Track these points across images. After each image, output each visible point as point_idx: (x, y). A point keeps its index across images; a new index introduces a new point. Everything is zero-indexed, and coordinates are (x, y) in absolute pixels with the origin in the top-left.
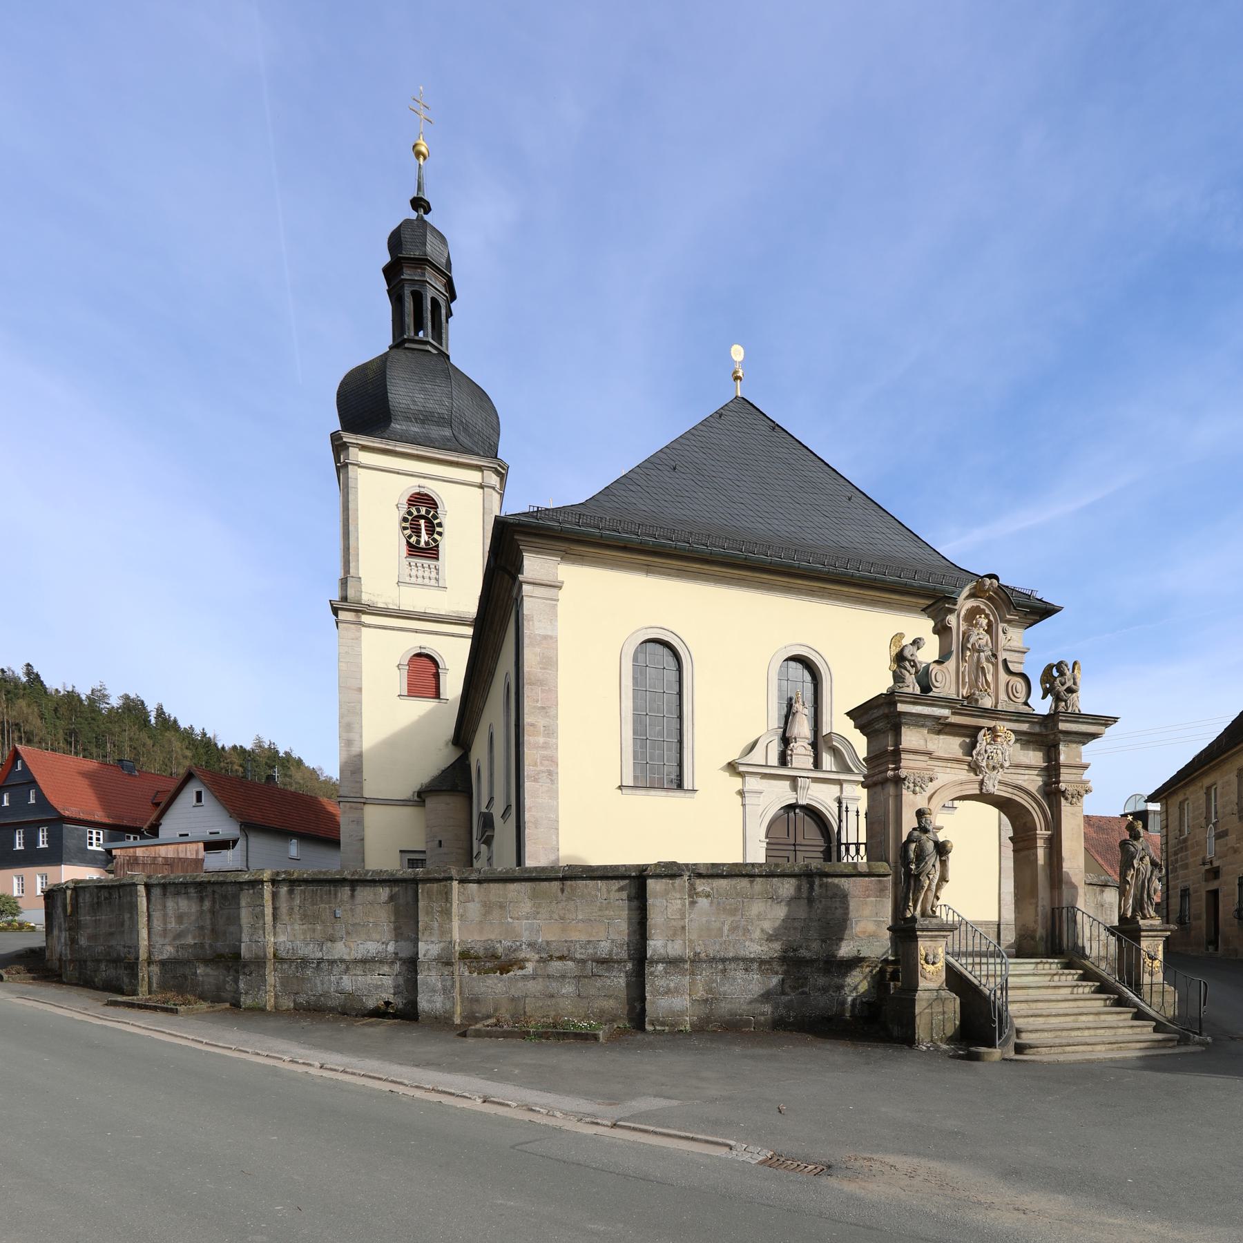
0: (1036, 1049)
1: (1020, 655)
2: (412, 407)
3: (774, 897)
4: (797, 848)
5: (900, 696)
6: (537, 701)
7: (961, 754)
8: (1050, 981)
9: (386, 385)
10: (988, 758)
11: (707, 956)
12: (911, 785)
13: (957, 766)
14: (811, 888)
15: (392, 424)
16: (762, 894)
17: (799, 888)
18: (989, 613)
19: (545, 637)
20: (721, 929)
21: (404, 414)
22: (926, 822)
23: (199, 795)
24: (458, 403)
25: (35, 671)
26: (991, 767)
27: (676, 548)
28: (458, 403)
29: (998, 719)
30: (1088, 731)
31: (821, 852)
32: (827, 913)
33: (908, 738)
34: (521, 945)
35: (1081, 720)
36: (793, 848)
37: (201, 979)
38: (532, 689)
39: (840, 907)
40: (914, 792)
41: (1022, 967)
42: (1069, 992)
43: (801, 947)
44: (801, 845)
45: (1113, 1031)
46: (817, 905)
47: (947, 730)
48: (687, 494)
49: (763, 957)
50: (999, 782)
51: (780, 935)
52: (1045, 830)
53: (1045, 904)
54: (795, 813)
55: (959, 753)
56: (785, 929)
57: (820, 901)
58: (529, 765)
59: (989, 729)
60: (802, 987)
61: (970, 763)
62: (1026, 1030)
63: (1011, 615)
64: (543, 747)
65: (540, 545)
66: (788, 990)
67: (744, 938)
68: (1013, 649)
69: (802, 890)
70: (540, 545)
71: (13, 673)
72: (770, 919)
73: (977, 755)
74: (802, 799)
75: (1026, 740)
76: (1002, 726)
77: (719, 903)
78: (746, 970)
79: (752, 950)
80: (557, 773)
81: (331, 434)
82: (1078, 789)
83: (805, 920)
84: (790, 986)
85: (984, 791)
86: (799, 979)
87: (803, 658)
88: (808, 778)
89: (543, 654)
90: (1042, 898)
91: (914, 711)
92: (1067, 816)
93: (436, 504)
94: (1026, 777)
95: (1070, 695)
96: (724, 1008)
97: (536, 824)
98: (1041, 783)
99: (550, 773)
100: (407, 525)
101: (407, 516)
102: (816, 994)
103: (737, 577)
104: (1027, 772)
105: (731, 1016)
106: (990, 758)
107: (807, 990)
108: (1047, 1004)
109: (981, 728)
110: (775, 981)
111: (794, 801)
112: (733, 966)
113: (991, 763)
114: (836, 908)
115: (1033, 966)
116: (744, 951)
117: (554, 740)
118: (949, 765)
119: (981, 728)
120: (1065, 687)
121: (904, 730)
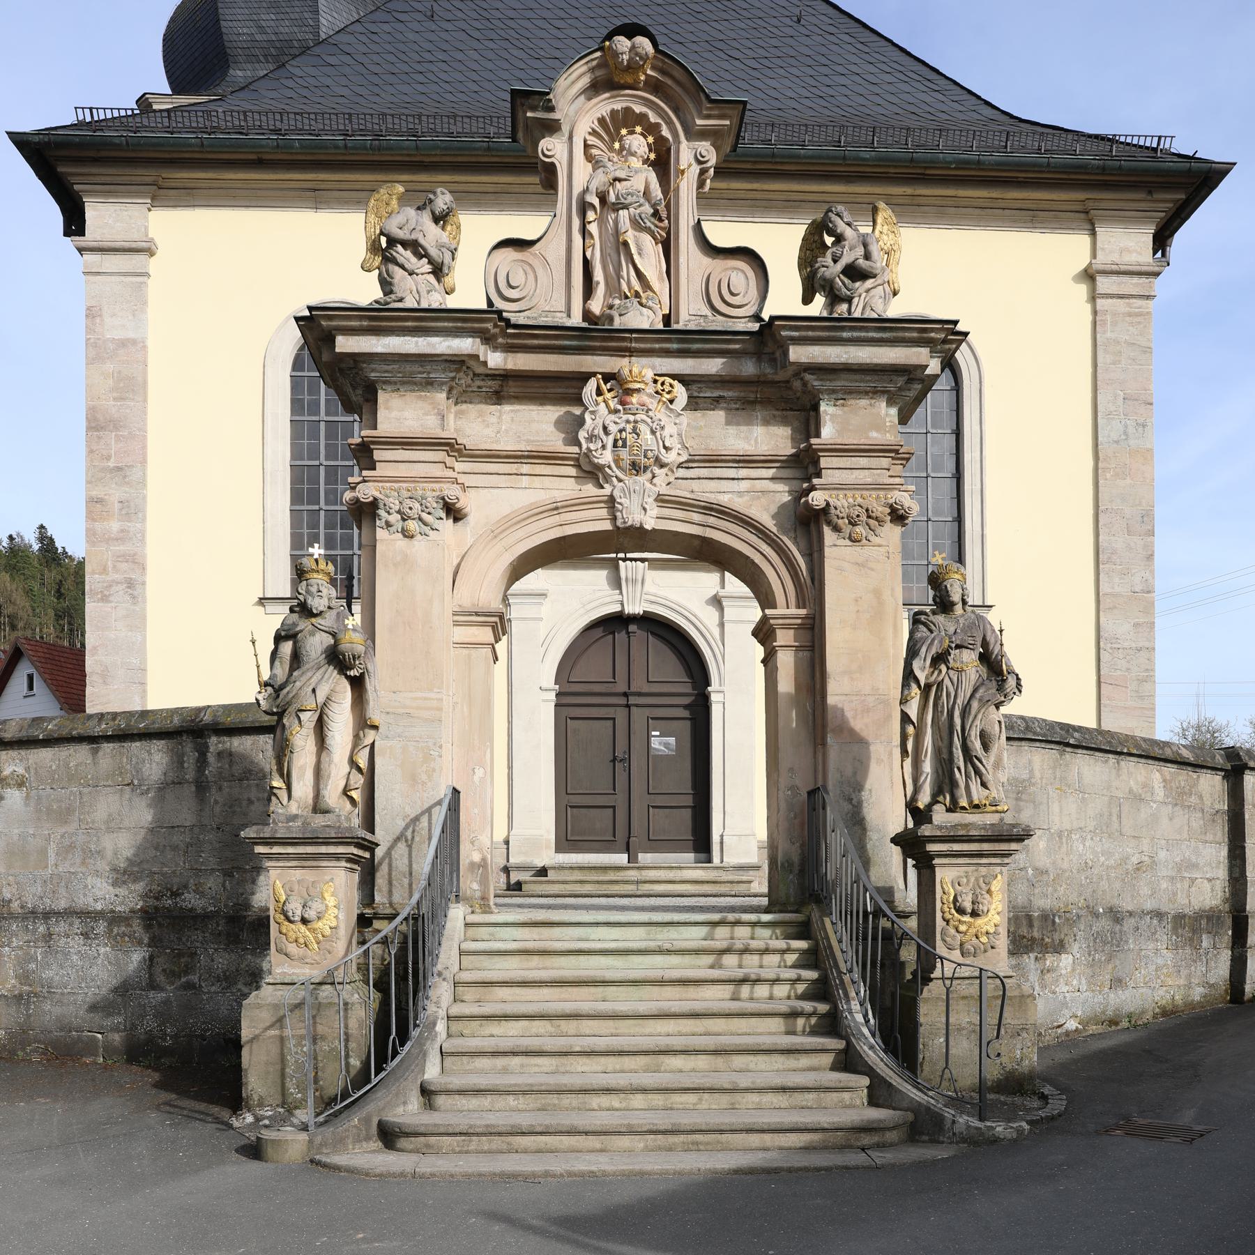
0: (422, 1139)
1: (1143, 280)
2: (258, 37)
3: (136, 782)
4: (632, 700)
5: (330, 318)
6: (108, 458)
7: (560, 443)
8: (712, 967)
9: (217, 9)
10: (615, 446)
11: (22, 907)
12: (394, 518)
14: (202, 761)
15: (231, 71)
16: (114, 775)
17: (178, 761)
18: (660, 121)
19: (123, 343)
20: (43, 852)
21: (247, 52)
22: (308, 592)
23: (30, 678)
24: (330, 19)
25: (49, 534)
26: (626, 463)
27: (346, 147)
28: (330, 19)
29: (631, 352)
30: (876, 361)
31: (686, 707)
33: (394, 414)
35: (845, 335)
36: (623, 701)
38: (99, 438)
39: (258, 800)
40: (407, 535)
41: (673, 933)
42: (728, 996)
43: (186, 887)
44: (640, 694)
45: (724, 1100)
46: (214, 795)
47: (512, 388)
48: (441, 56)
49: (118, 909)
50: (656, 500)
51: (148, 861)
52: (798, 607)
53: (798, 782)
54: (628, 633)
55: (555, 442)
56: (156, 849)
57: (220, 789)
58: (93, 573)
59: (607, 377)
60: (186, 973)
61: (577, 460)
62: (443, 1088)
63: (708, 117)
64: (117, 539)
65: (108, 179)
66: (160, 978)
67: (84, 870)
68: (1123, 268)
69: (186, 765)
70: (108, 179)
71: (22, 540)
72: (128, 829)
73: (591, 438)
74: (634, 603)
75: (738, 399)
76: (642, 369)
77: (39, 798)
78: (85, 935)
79: (99, 894)
80: (144, 583)
81: (137, 102)
82: (865, 504)
84: (164, 970)
85: (619, 523)
86: (180, 955)
88: (643, 560)
89: (120, 372)
90: (791, 770)
91: (379, 349)
92: (840, 569)
94: (744, 485)
95: (858, 284)
96: (49, 1012)
97: (105, 677)
98: (786, 498)
99: (130, 584)
102: (213, 989)
103: (490, 188)
104: (743, 473)
105: (61, 1030)
106: (620, 443)
107: (196, 980)
108: (610, 1023)
109: (585, 377)
110: (137, 957)
111: (617, 608)
112: (62, 927)
113: (624, 454)
114: (250, 802)
115: (703, 931)
116: (85, 895)
117: (138, 525)
118: (525, 469)
119: (585, 377)
120: (840, 266)
121: (381, 396)
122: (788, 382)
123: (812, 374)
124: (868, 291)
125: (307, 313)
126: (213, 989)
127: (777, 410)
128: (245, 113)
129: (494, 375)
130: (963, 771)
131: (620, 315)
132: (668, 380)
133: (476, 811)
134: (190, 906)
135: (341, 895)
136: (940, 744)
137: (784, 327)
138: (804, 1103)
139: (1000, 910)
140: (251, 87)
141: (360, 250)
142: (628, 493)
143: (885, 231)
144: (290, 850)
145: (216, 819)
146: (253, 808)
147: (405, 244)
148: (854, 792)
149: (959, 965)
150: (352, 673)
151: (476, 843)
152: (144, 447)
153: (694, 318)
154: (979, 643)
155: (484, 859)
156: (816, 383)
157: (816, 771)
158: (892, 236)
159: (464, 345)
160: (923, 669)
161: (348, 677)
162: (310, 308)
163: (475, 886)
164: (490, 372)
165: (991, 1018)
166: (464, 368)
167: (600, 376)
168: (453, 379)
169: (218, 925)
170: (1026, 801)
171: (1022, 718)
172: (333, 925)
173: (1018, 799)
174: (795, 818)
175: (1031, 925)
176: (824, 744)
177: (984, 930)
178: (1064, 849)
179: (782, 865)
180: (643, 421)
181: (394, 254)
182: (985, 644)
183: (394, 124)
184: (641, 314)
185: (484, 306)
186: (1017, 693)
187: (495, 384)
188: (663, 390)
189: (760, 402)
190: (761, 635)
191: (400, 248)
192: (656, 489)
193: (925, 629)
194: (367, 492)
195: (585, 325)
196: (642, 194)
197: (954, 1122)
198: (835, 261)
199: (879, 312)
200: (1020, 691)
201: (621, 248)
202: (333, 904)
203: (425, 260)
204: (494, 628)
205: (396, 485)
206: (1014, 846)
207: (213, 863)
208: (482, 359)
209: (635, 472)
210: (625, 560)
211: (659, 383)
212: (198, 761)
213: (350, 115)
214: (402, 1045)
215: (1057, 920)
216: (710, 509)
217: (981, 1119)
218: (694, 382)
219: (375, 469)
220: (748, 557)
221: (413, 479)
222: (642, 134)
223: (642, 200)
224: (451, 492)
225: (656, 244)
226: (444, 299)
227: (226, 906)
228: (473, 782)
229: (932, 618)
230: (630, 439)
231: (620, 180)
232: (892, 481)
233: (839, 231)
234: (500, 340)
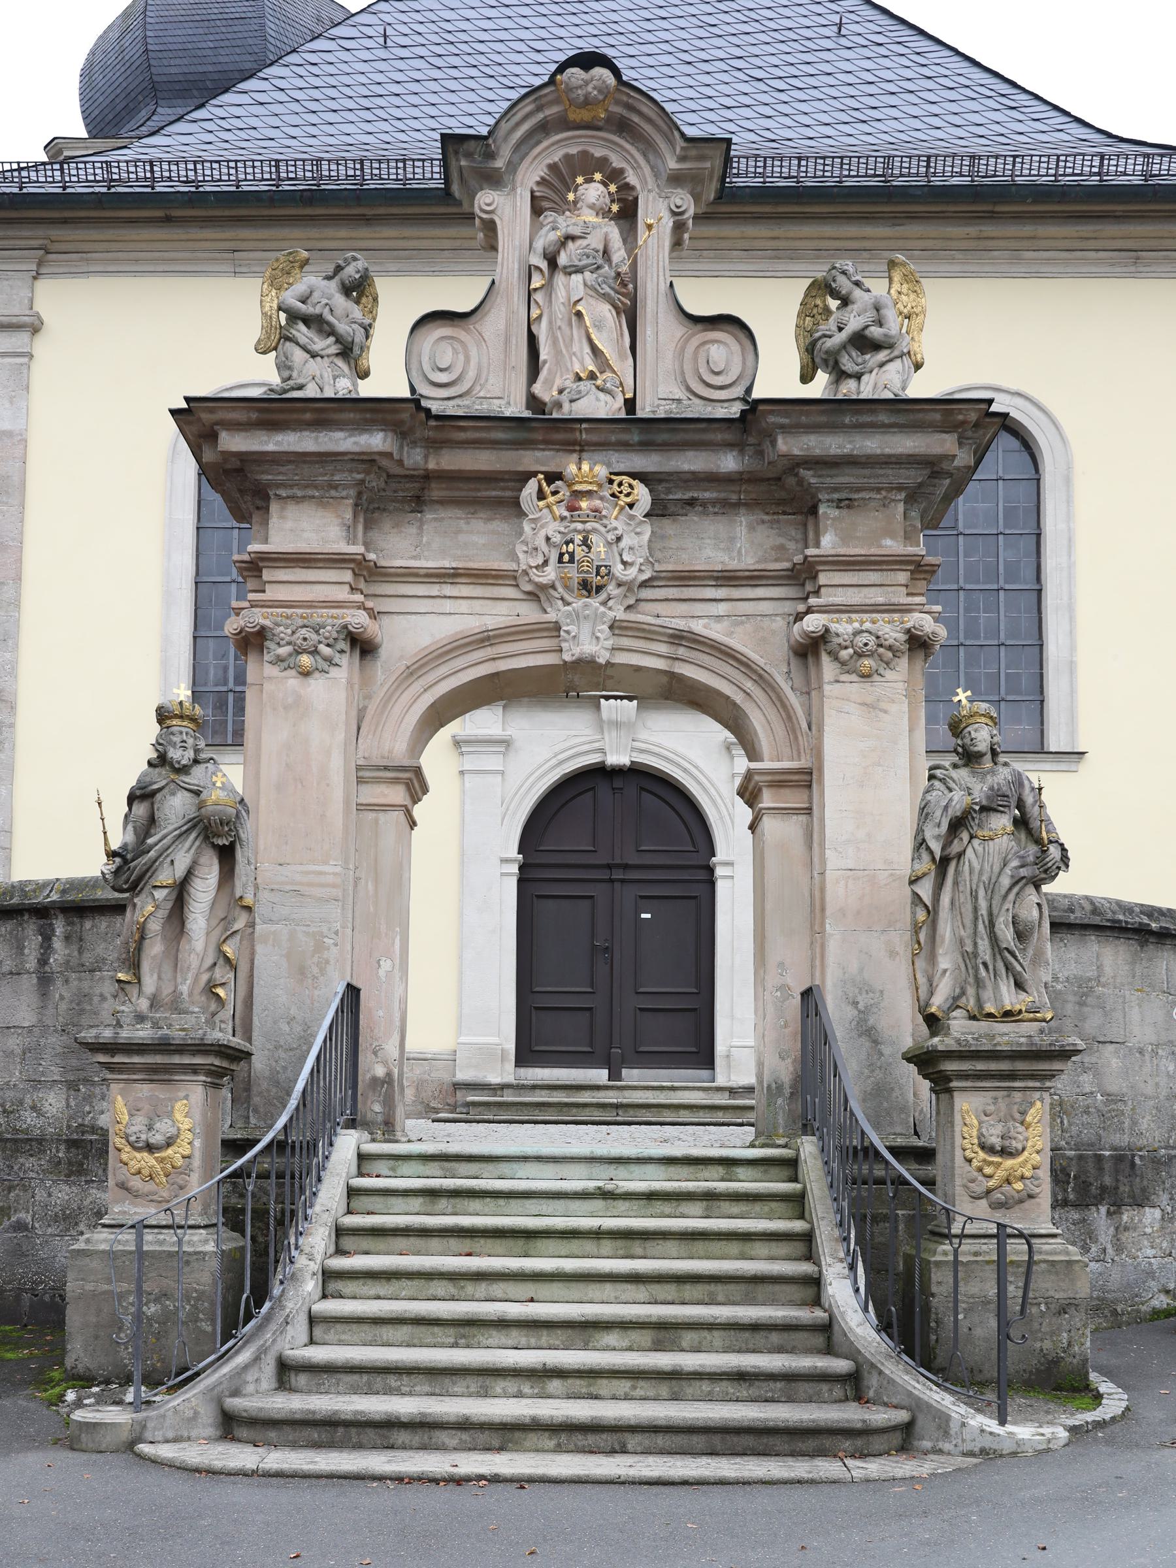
10: (560, 561)
13: (478, 591)
32: (83, 1011)
37: (21, 1160)
46: (59, 990)
53: (789, 980)
57: (67, 981)
59: (552, 477)
69: (26, 951)
81: (45, 147)
83: (30, 1029)
94: (722, 608)
95: (867, 357)
102: (50, 1230)
106: (566, 558)
114: (103, 998)
121: (274, 507)
122: (779, 479)
123: (809, 469)
124: (882, 365)
125: (184, 405)
126: (50, 1230)
127: (767, 514)
128: (151, 163)
129: (413, 476)
130: (991, 967)
131: (572, 401)
132: (626, 479)
133: (381, 1013)
134: (24, 1126)
135: (198, 1117)
136: (962, 933)
137: (771, 412)
138: (770, 1394)
139: (1038, 1147)
140: (163, 132)
141: (254, 330)
142: (577, 617)
143: (905, 290)
144: (136, 1059)
145: (61, 1019)
146: (106, 1005)
147: (307, 320)
148: (860, 993)
149: (970, 1218)
150: (221, 842)
151: (379, 1054)
152: (20, 560)
153: (663, 402)
154: (1013, 804)
155: (389, 1074)
156: (813, 480)
157: (812, 967)
158: (913, 296)
159: (376, 441)
160: (938, 837)
161: (215, 846)
162: (187, 399)
163: (377, 1108)
164: (407, 473)
165: (1014, 1290)
166: (376, 468)
167: (541, 476)
168: (363, 481)
169: (58, 1151)
170: (1093, 1007)
171: (1087, 898)
172: (186, 1153)
173: (1082, 1004)
174: (786, 1026)
175: (1101, 1169)
176: (822, 932)
177: (1018, 1173)
178: (1147, 1069)
179: (769, 1087)
180: (595, 530)
181: (294, 332)
182: (1020, 805)
183: (330, 170)
184: (598, 399)
185: (406, 394)
186: (1063, 868)
187: (412, 487)
188: (621, 492)
189: (746, 505)
190: (747, 795)
191: (302, 327)
192: (611, 614)
193: (943, 787)
194: (258, 618)
195: (527, 414)
196: (601, 254)
197: (963, 1425)
198: (840, 329)
199: (897, 391)
200: (1067, 866)
201: (574, 318)
202: (187, 1127)
203: (332, 339)
204: (409, 786)
205: (289, 611)
206: (1057, 1065)
207: (55, 1074)
208: (396, 456)
209: (585, 592)
210: (607, 698)
211: (616, 483)
212: (41, 947)
213: (277, 161)
214: (259, 1305)
215: (1137, 1161)
216: (678, 638)
217: (1002, 1422)
218: (660, 481)
219: (264, 591)
220: (728, 697)
221: (310, 605)
222: (576, 191)
223: (600, 261)
224: (358, 619)
225: (618, 313)
226: (355, 385)
227: (69, 1127)
228: (378, 978)
229: (954, 774)
230: (580, 552)
231: (573, 238)
232: (910, 600)
233: (844, 292)
234: (418, 435)
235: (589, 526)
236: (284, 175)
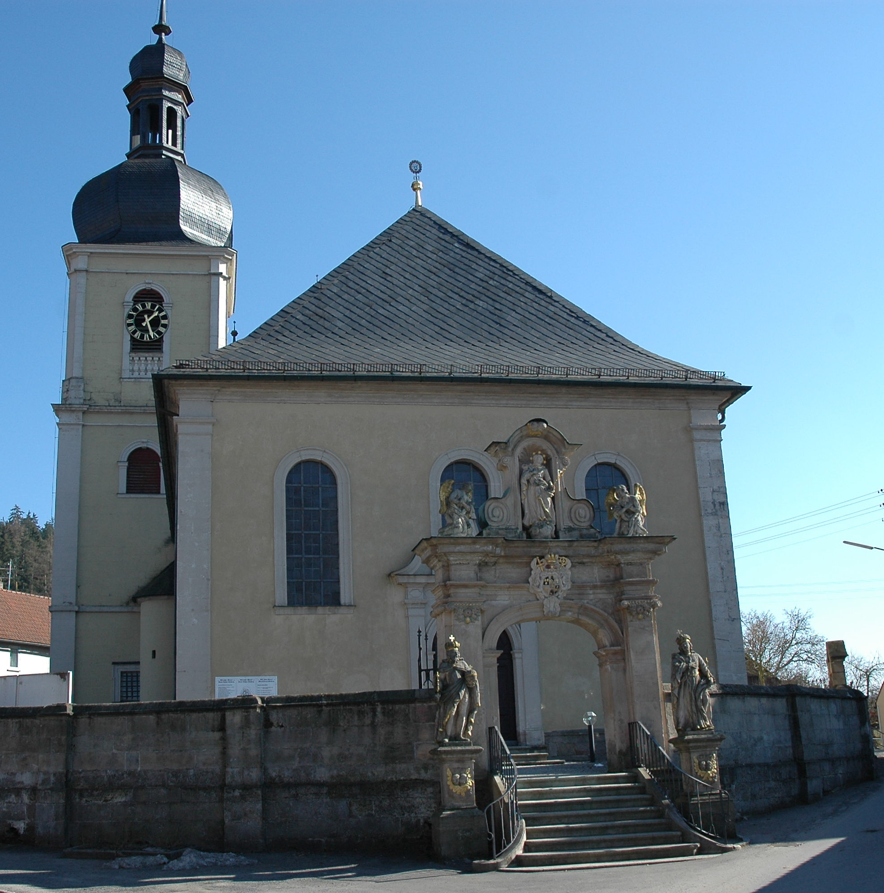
10: (544, 584)
34: (123, 775)
87: (463, 461)
93: (162, 298)
100: (131, 321)
101: (132, 313)
106: (546, 583)
132: (564, 558)
174: (623, 732)
230: (550, 581)
235: (553, 573)
236: (286, 369)
